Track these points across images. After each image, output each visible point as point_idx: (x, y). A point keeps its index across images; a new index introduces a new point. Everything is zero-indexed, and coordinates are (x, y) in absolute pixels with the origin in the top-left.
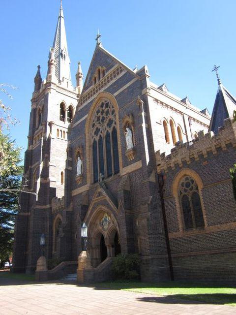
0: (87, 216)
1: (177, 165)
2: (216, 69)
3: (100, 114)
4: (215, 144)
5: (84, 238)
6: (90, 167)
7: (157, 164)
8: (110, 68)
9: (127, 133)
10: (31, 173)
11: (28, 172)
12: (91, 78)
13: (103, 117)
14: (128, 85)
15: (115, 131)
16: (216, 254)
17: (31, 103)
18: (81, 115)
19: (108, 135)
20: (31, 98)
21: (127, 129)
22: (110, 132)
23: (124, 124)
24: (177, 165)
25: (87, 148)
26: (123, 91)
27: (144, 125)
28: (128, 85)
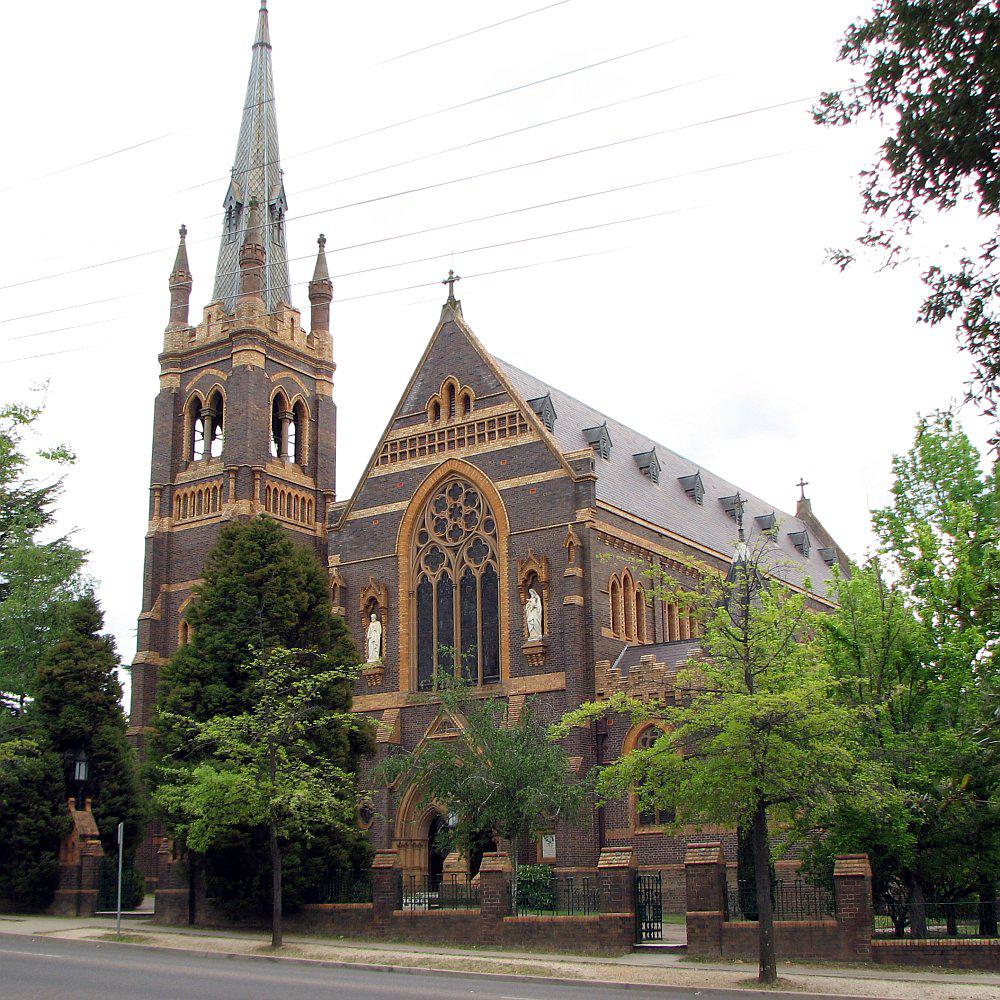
3: (446, 514)
5: (81, 782)
6: (408, 649)
7: (597, 692)
8: (617, 657)
9: (533, 600)
10: (167, 610)
11: (158, 604)
12: (421, 398)
13: (455, 525)
14: (540, 477)
15: (490, 578)
16: (865, 979)
17: (157, 369)
18: (384, 496)
19: (467, 581)
20: (160, 350)
22: (477, 574)
25: (402, 598)
26: (525, 488)
28: (540, 477)
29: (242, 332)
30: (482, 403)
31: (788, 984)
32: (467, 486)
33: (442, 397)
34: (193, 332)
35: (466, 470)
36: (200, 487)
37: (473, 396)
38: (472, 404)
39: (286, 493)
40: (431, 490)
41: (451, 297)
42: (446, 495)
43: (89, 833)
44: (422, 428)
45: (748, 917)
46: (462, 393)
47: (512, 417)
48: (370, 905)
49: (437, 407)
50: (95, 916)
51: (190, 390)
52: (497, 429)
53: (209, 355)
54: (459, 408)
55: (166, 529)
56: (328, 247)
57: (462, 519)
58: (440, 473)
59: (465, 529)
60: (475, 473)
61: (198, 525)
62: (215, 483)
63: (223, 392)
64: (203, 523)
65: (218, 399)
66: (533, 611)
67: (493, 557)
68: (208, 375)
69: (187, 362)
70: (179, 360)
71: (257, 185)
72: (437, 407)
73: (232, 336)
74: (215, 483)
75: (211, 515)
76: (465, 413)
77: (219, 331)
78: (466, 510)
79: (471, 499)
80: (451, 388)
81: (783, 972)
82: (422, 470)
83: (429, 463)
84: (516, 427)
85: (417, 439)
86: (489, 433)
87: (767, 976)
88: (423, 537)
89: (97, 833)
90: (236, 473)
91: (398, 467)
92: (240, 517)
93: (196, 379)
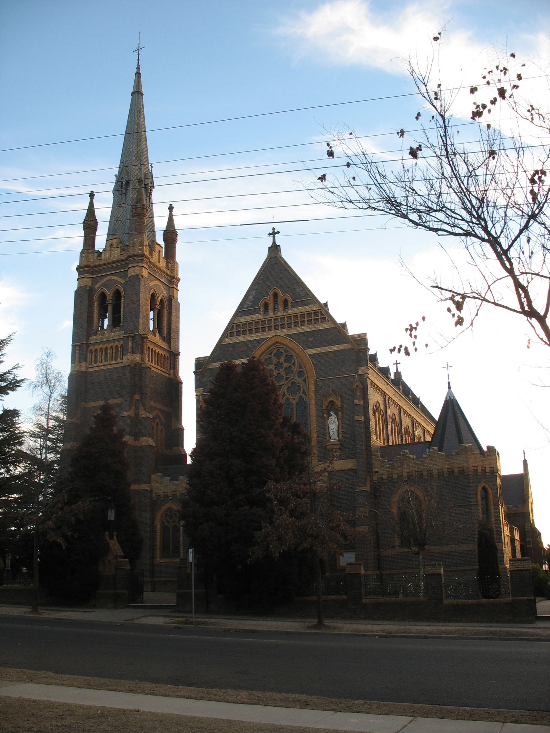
0: (526, 568)
1: (400, 477)
2: (448, 367)
4: (448, 467)
14: (335, 348)
21: (332, 413)
23: (325, 404)
24: (400, 477)
27: (503, 533)
28: (335, 348)
29: (136, 255)
30: (295, 305)
31: (327, 627)
32: (286, 351)
33: (270, 299)
34: (99, 254)
35: (286, 342)
36: (106, 345)
37: (290, 299)
38: (290, 304)
39: (157, 352)
40: (263, 353)
41: (274, 243)
42: (272, 356)
43: (119, 554)
44: (257, 317)
45: (485, 597)
46: (283, 298)
47: (316, 313)
48: (344, 597)
49: (266, 305)
50: (128, 607)
51: (99, 288)
52: (306, 319)
53: (112, 268)
54: (281, 306)
55: (84, 369)
56: (174, 212)
57: (283, 370)
58: (269, 343)
59: (285, 376)
60: (293, 344)
61: (106, 367)
62: (117, 343)
63: (122, 290)
64: (110, 367)
65: (117, 295)
66: (333, 425)
67: (304, 392)
68: (111, 280)
69: (96, 271)
70: (91, 269)
71: (137, 172)
72: (266, 305)
73: (129, 257)
74: (117, 343)
75: (114, 362)
76: (284, 310)
77: (119, 254)
78: (285, 365)
79: (289, 358)
80: (275, 295)
81: (327, 622)
82: (258, 341)
83: (262, 337)
84: (298, 322)
85: (254, 323)
86: (301, 322)
87: (320, 623)
88: (305, 380)
89: (123, 554)
90: (132, 337)
91: (241, 339)
92: (135, 364)
93: (103, 281)
